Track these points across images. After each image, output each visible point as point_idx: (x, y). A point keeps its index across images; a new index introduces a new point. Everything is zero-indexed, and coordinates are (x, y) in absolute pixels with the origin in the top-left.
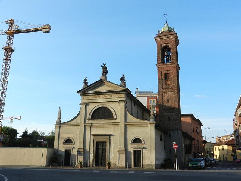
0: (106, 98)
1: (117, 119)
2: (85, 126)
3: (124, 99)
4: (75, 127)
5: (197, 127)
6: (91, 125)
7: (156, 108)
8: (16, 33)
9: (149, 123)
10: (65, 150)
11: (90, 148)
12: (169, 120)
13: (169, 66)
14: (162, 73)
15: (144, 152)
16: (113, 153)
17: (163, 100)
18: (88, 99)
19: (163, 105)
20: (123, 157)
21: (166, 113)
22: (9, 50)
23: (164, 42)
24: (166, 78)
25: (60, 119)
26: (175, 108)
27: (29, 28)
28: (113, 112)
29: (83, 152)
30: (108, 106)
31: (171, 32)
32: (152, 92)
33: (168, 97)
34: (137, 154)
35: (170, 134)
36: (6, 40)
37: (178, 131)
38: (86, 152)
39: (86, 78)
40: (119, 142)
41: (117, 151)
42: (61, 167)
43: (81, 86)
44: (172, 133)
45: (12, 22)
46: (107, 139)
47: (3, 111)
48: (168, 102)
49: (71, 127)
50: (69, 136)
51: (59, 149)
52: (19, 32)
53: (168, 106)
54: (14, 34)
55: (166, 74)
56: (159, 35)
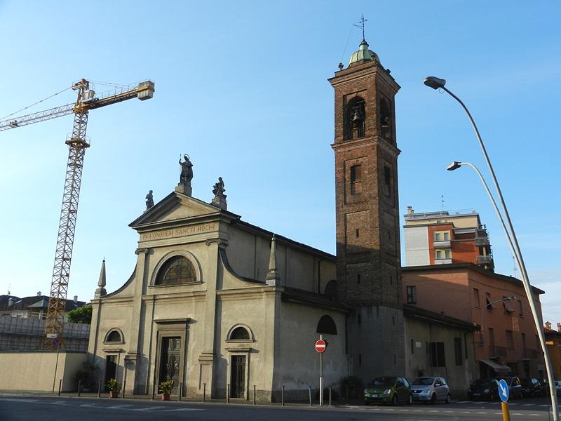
1: (202, 282)
2: (143, 301)
3: (216, 235)
4: (126, 305)
5: (488, 294)
6: (155, 300)
7: (451, 253)
8: (91, 108)
9: (262, 290)
10: (108, 357)
11: (151, 350)
12: (359, 282)
13: (362, 146)
14: (345, 166)
15: (251, 360)
16: (192, 364)
17: (346, 232)
18: (154, 240)
19: (346, 245)
20: (209, 371)
21: (353, 263)
22: (78, 145)
23: (352, 90)
24: (353, 178)
25: (105, 287)
26: (372, 249)
27: (112, 93)
28: (196, 268)
29: (137, 362)
30: (185, 252)
31: (370, 60)
32: (447, 214)
33: (357, 224)
34: (238, 364)
35: (360, 317)
36: (72, 123)
37: (378, 308)
38: (143, 360)
39: (151, 192)
40: (203, 338)
41: (198, 358)
42: (95, 396)
43: (142, 209)
44: (364, 312)
45: (84, 84)
46: (181, 329)
47: (68, 275)
48: (358, 235)
49: (119, 305)
50: (246, 322)
51: (97, 354)
52: (96, 104)
53: (358, 247)
54: (89, 110)
55: (353, 168)
56: (343, 73)
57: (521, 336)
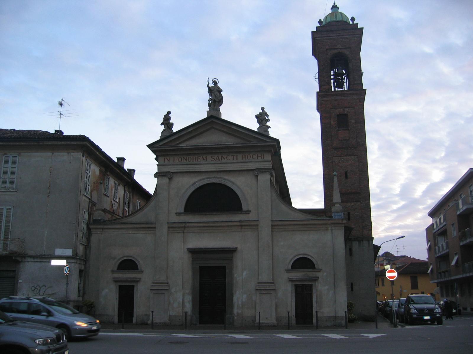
0: (223, 161)
39: (169, 113)
48: (346, 177)
50: (311, 253)
57: (14, 269)
